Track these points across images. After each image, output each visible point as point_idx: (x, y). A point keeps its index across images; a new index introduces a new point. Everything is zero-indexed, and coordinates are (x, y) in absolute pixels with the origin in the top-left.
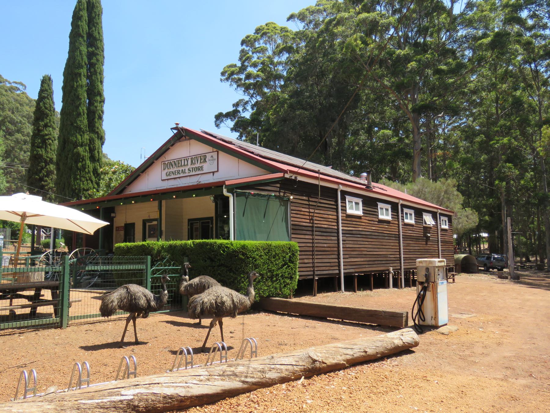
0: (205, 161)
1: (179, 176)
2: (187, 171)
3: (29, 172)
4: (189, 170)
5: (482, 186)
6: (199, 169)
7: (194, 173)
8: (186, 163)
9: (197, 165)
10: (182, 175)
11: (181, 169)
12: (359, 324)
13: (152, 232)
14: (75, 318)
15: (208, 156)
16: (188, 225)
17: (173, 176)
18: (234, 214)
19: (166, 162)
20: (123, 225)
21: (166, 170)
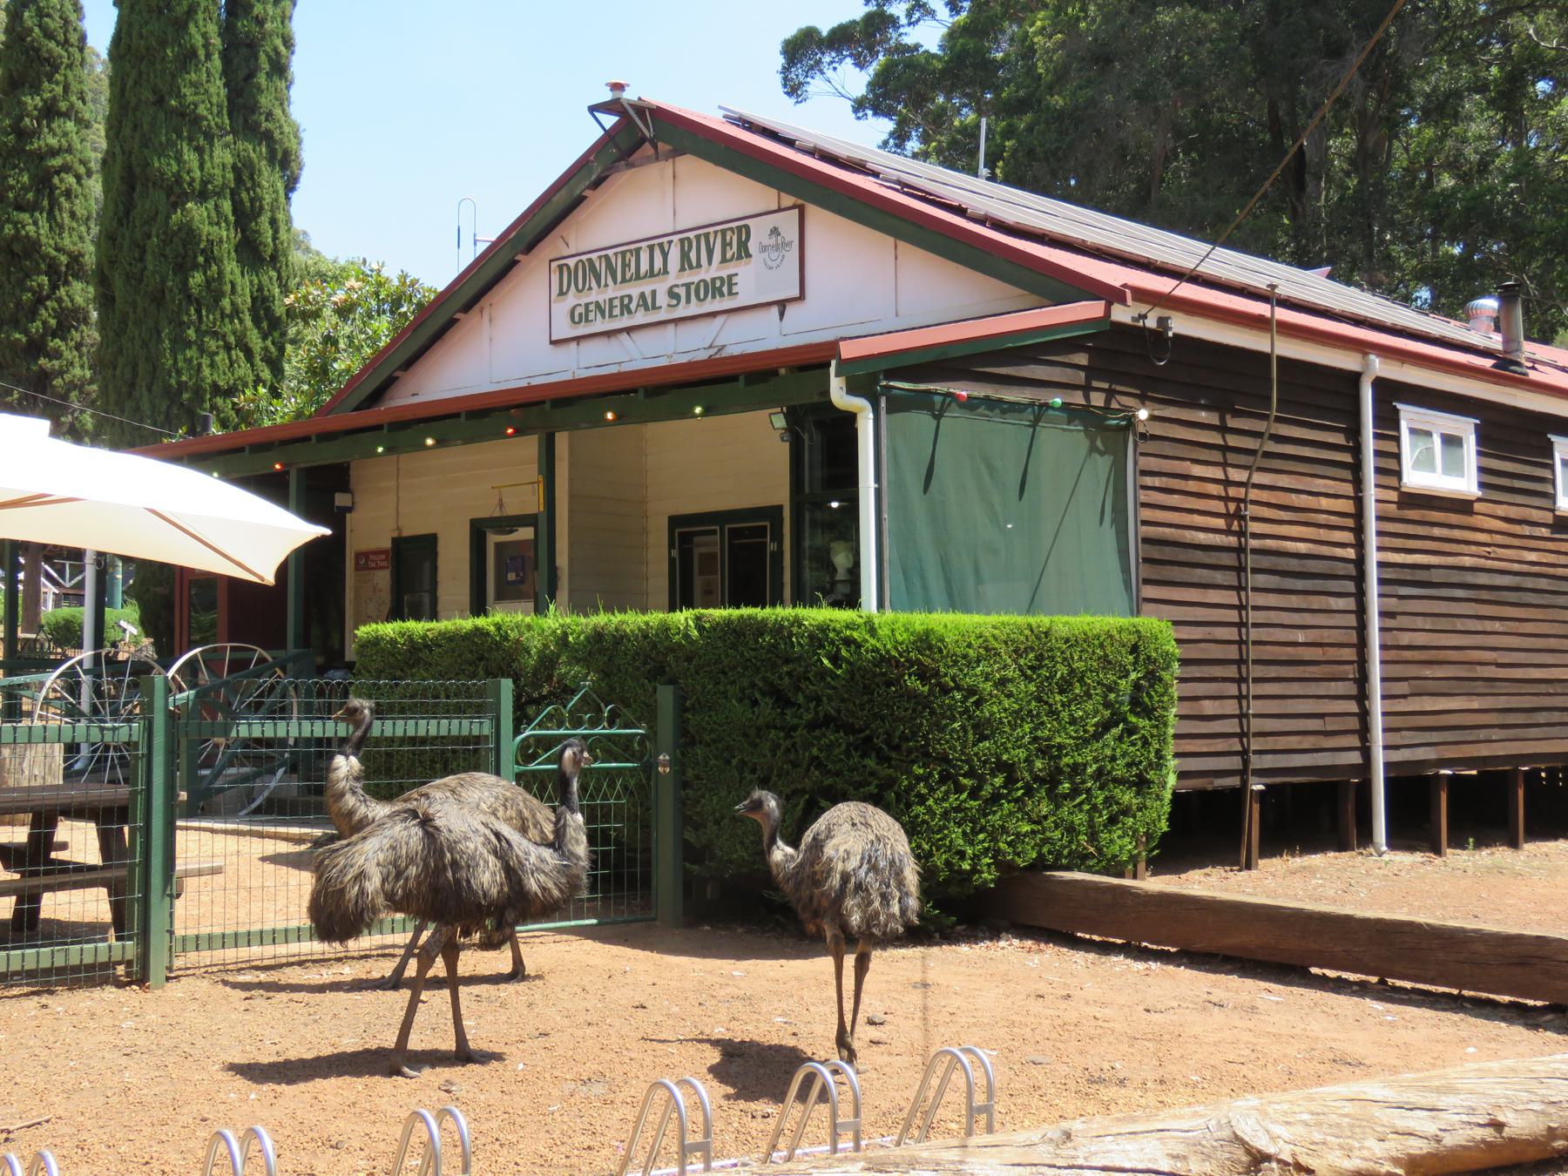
0: (744, 252)
2: (662, 299)
6: (715, 288)
7: (694, 308)
8: (658, 264)
10: (640, 318)
11: (634, 290)
13: (512, 576)
15: (759, 231)
16: (671, 546)
19: (571, 262)
21: (572, 299)
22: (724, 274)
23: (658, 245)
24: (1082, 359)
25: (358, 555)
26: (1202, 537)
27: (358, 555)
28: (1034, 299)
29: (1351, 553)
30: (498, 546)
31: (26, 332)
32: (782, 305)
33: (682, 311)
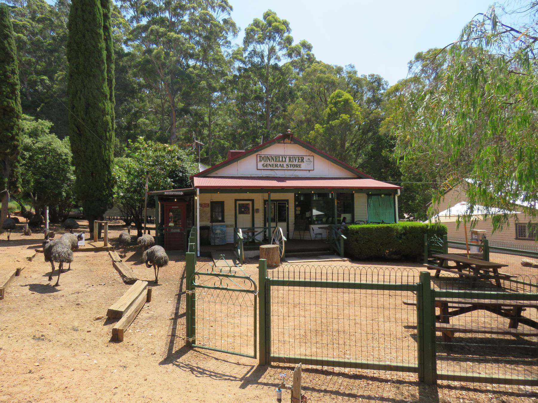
0: (302, 161)
1: (276, 168)
2: (285, 166)
3: (104, 161)
4: (287, 165)
5: (352, 121)
6: (296, 166)
7: (292, 168)
8: (284, 159)
9: (296, 163)
10: (280, 168)
11: (279, 163)
12: (471, 294)
13: (243, 210)
14: (279, 360)
15: (306, 159)
16: (288, 208)
17: (270, 168)
18: (374, 223)
19: (263, 156)
20: (209, 202)
21: (263, 162)
22: (299, 164)
23: (284, 157)
24: (450, 310)
25: (249, 213)
26: (456, 300)
27: (249, 213)
28: (349, 174)
29: (443, 368)
30: (239, 204)
31: (11, 133)
32: (309, 170)
33: (289, 168)
